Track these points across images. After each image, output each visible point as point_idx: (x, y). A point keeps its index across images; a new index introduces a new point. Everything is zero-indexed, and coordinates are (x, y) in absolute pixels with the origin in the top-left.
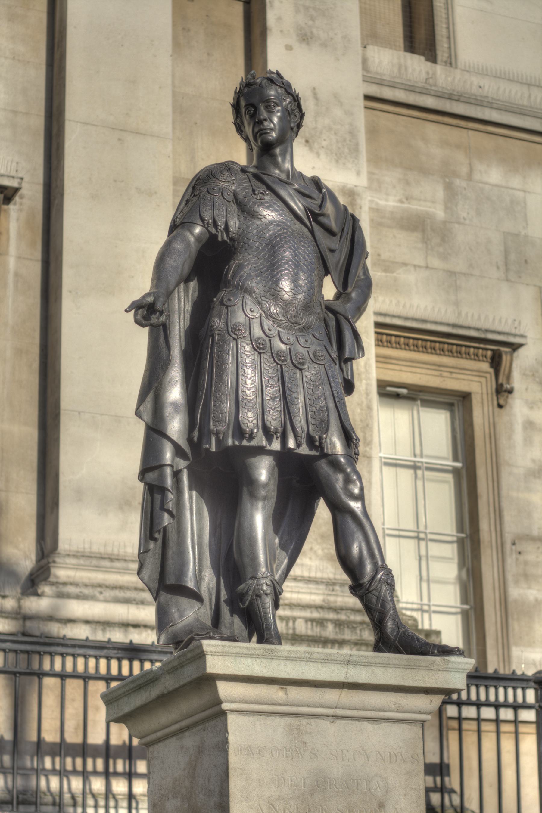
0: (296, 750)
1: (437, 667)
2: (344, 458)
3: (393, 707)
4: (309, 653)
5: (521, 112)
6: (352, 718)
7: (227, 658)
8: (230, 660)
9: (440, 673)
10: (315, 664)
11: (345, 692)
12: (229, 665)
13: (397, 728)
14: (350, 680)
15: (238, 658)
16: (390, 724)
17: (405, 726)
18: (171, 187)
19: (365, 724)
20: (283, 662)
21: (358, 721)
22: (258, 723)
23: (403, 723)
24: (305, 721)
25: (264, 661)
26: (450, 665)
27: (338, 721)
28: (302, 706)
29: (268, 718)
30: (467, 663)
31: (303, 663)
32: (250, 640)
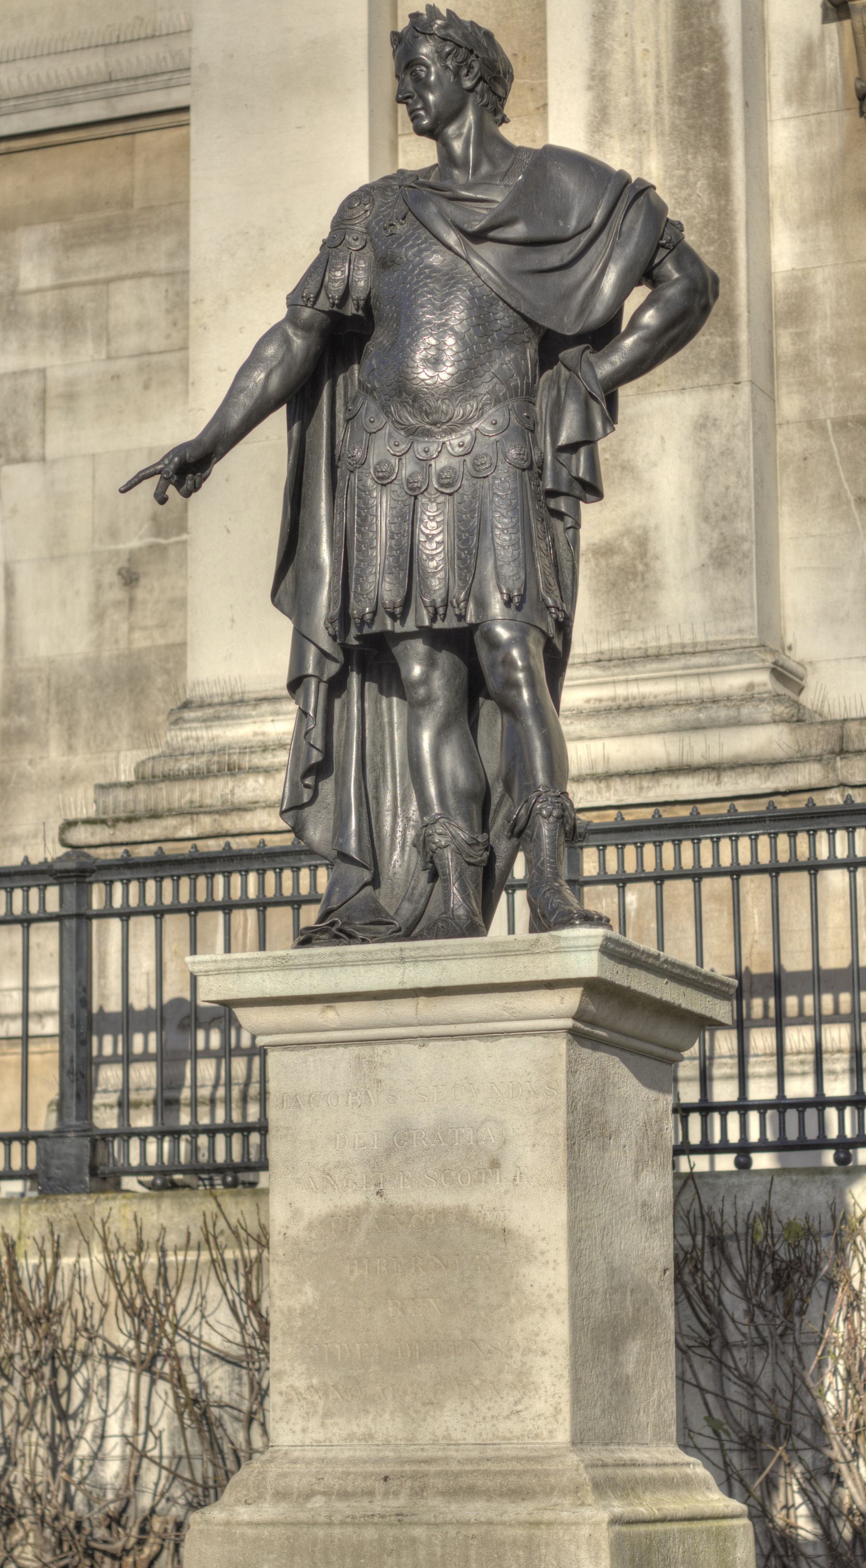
0: (366, 1093)
1: (544, 949)
2: (508, 627)
3: (506, 1014)
4: (338, 954)
5: (58, 95)
6: (452, 1037)
7: (227, 976)
8: (230, 978)
9: (553, 956)
10: (355, 968)
11: (422, 1001)
12: (231, 986)
13: (524, 1044)
14: (408, 986)
15: (242, 975)
16: (514, 1039)
17: (539, 1039)
18: (194, 264)
19: (474, 1042)
20: (307, 972)
21: (463, 1039)
22: (311, 1059)
23: (534, 1035)
24: (380, 1049)
25: (280, 974)
26: (563, 944)
27: (432, 1044)
28: (438, 1024)
29: (326, 1050)
30: (589, 937)
31: (337, 970)
32: (476, 925)
